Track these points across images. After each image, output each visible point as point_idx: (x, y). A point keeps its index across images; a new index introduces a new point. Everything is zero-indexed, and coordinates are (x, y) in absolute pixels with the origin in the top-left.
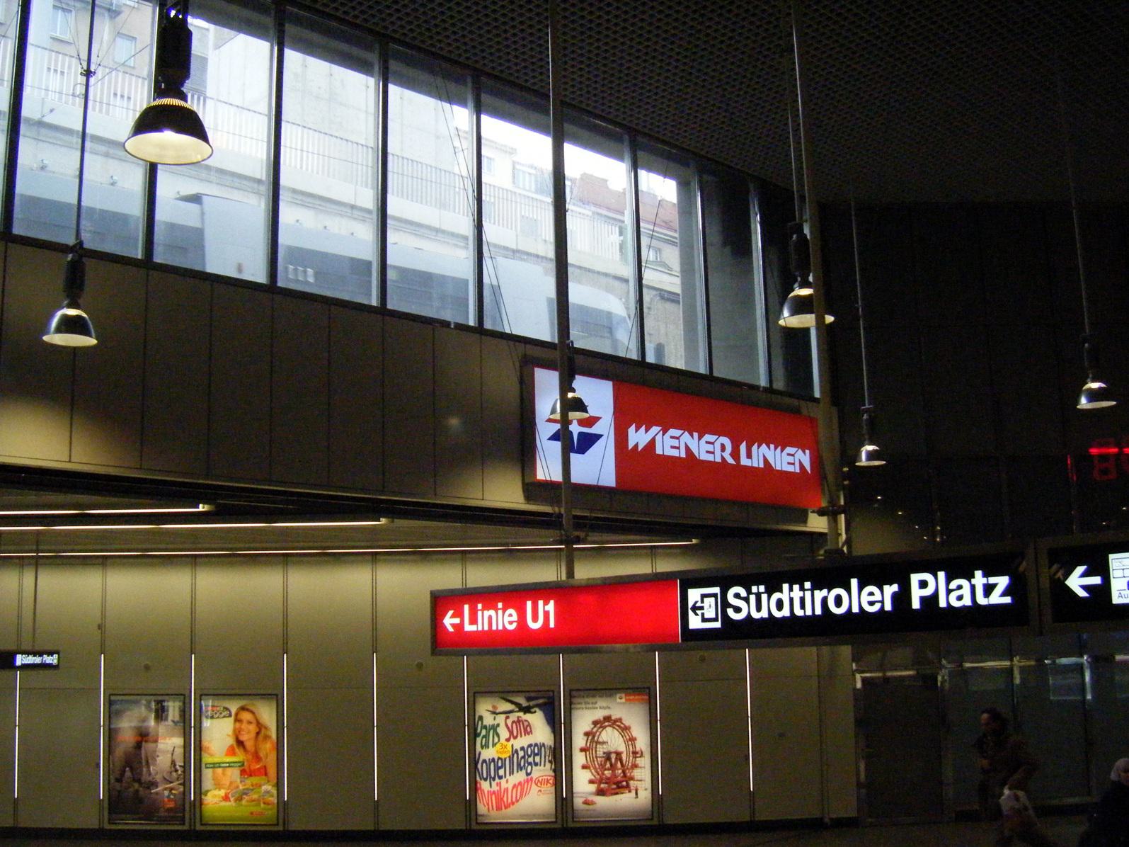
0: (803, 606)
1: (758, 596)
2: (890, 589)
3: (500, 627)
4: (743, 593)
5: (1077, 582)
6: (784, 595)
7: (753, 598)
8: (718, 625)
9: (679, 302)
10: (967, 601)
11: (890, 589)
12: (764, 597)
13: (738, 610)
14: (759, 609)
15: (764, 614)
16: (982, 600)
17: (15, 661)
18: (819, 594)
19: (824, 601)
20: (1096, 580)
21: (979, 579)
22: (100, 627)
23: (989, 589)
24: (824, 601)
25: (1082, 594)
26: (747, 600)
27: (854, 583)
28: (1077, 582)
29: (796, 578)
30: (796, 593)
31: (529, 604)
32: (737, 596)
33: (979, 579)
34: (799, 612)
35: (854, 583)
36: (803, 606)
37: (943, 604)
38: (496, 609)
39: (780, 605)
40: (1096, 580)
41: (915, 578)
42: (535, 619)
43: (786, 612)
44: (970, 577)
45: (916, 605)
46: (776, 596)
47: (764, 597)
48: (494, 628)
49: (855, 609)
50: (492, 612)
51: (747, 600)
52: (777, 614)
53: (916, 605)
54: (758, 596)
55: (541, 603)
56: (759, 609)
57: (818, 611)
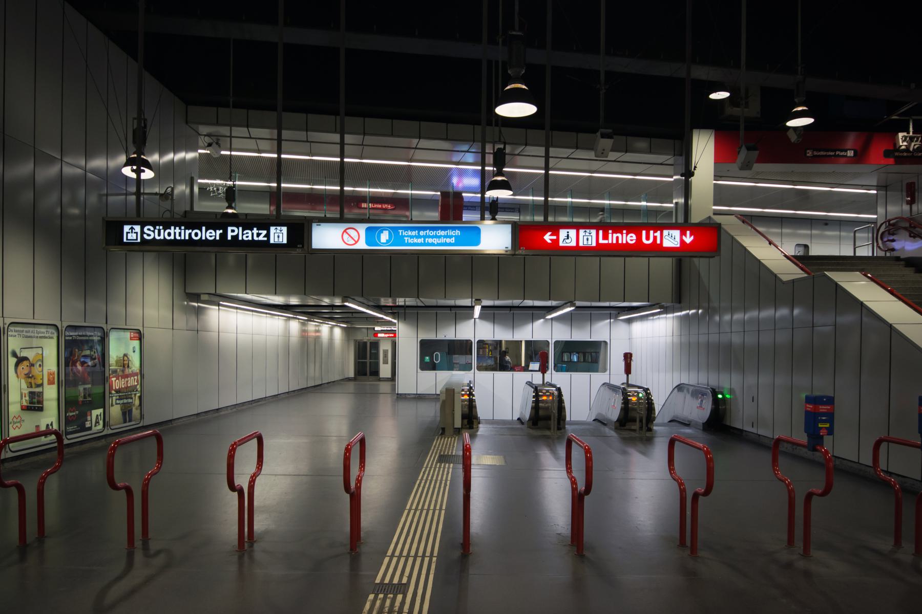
0: (180, 235)
1: (159, 231)
2: (219, 232)
3: (624, 242)
4: (152, 228)
5: (548, 237)
6: (172, 231)
7: (156, 231)
8: (125, 240)
9: (125, 422)
10: (250, 238)
11: (219, 232)
12: (162, 231)
13: (149, 235)
14: (159, 235)
15: (162, 237)
16: (256, 238)
17: (789, 140)
18: (188, 232)
19: (190, 234)
20: (554, 237)
21: (255, 231)
22: (469, 385)
23: (258, 235)
24: (190, 234)
25: (549, 242)
26: (154, 232)
27: (204, 228)
28: (548, 237)
29: (177, 224)
30: (178, 230)
31: (644, 233)
32: (149, 230)
33: (255, 231)
34: (178, 238)
35: (204, 228)
36: (180, 235)
37: (240, 238)
38: (622, 234)
39: (169, 234)
40: (554, 237)
41: (230, 229)
42: (648, 238)
43: (172, 237)
44: (252, 230)
45: (229, 238)
46: (167, 231)
47: (162, 231)
48: (620, 242)
49: (204, 238)
50: (619, 235)
51: (154, 232)
52: (167, 238)
53: (229, 238)
54: (159, 231)
55: (652, 232)
56: (159, 235)
57: (187, 238)
